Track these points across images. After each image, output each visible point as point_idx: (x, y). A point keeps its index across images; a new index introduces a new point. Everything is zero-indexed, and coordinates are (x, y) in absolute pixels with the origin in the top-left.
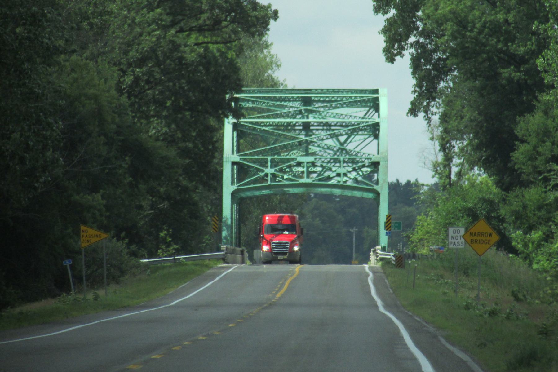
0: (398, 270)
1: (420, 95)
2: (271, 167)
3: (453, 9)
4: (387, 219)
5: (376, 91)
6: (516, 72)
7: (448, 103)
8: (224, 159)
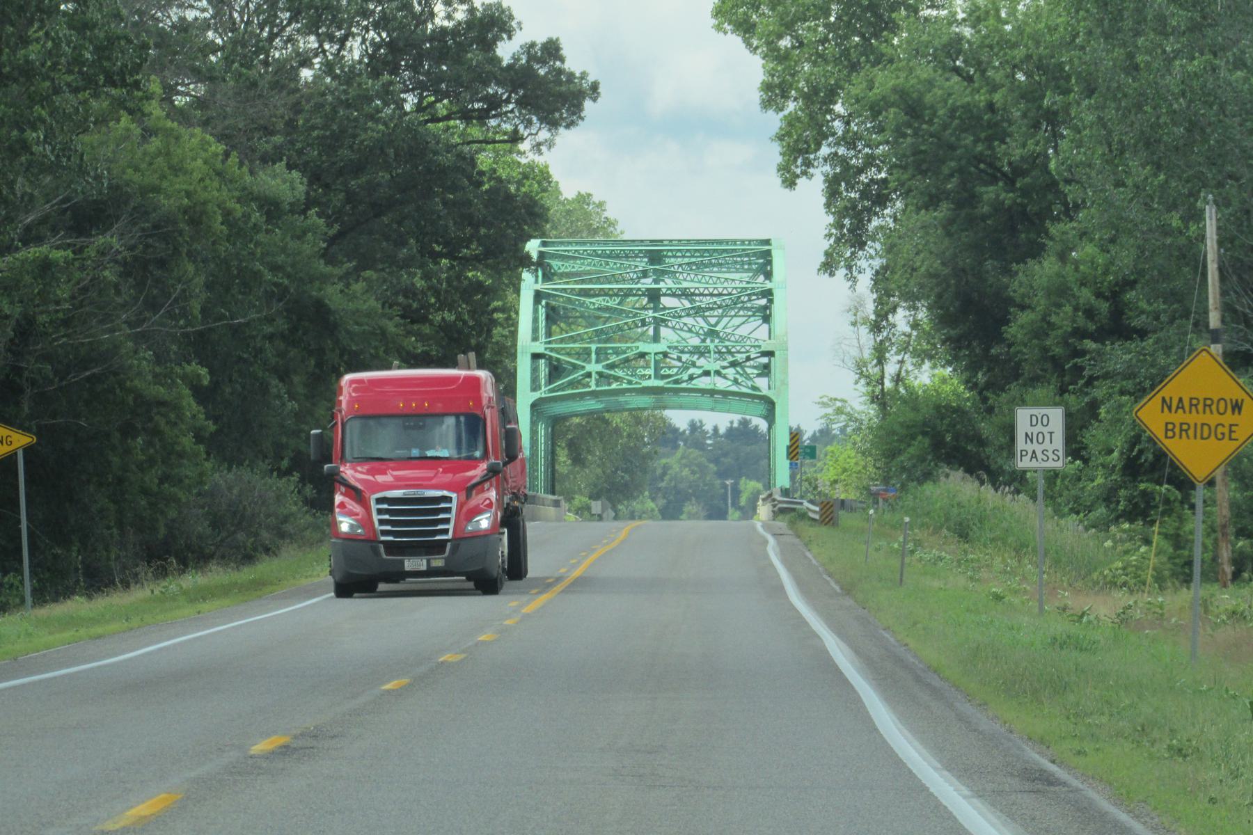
0: (824, 530)
1: (838, 240)
2: (598, 361)
3: (898, 85)
4: (791, 440)
5: (767, 242)
6: (1007, 192)
7: (890, 249)
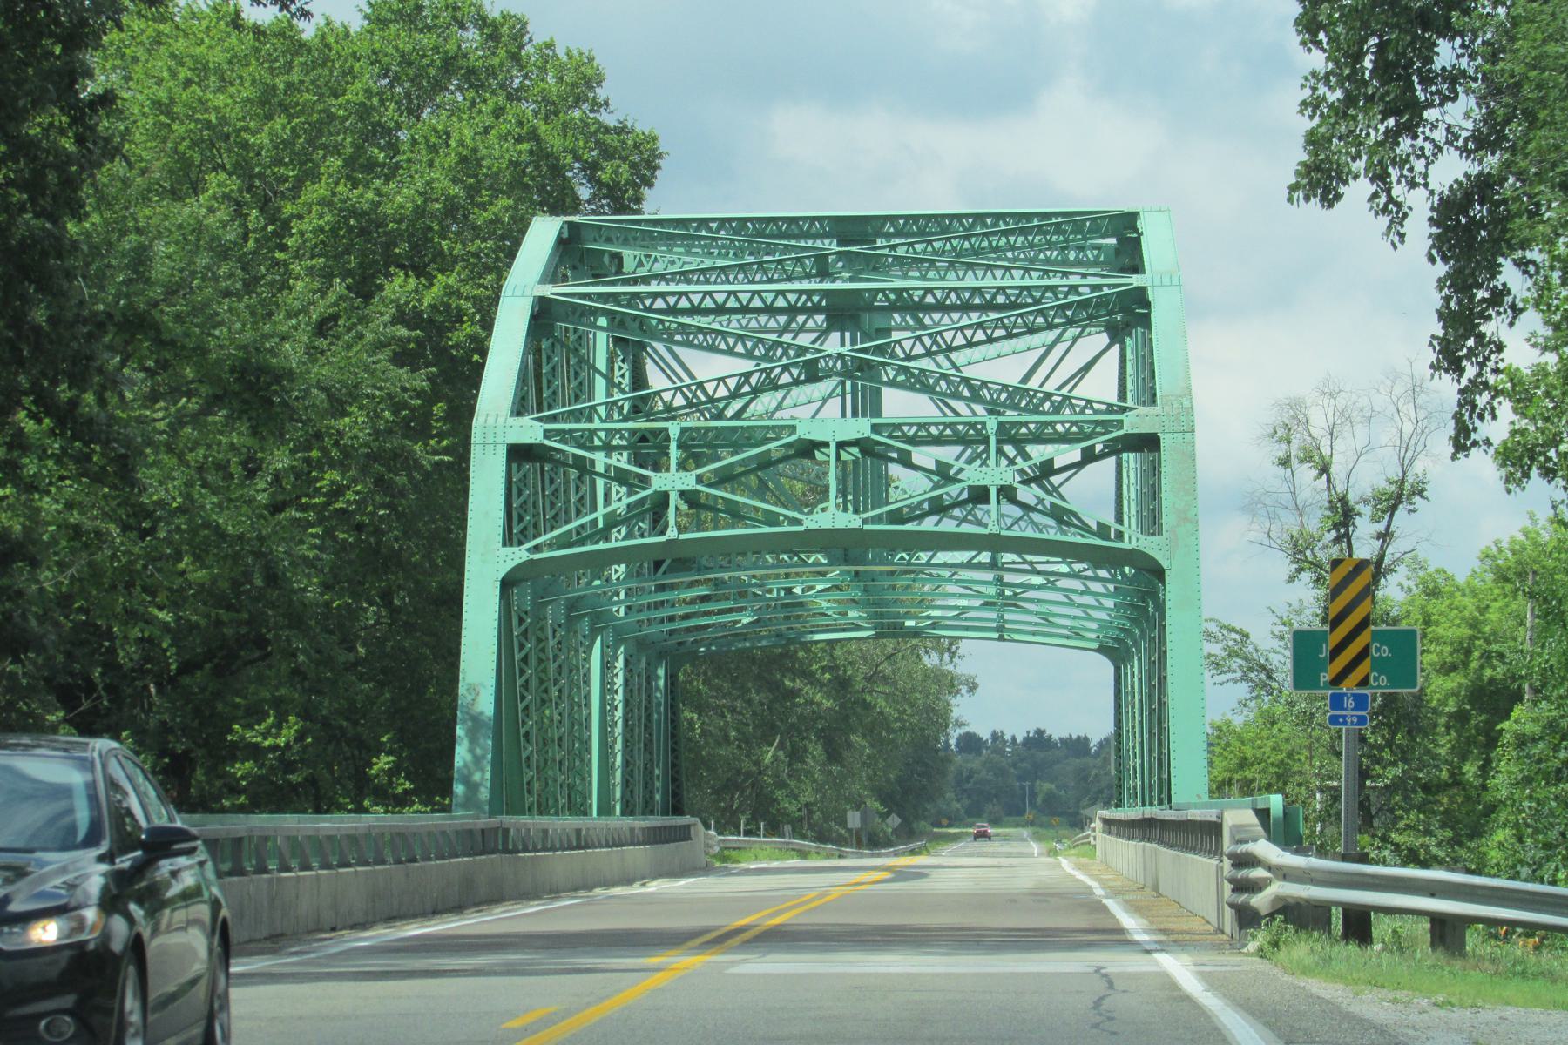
2: (682, 466)
8: (477, 435)
